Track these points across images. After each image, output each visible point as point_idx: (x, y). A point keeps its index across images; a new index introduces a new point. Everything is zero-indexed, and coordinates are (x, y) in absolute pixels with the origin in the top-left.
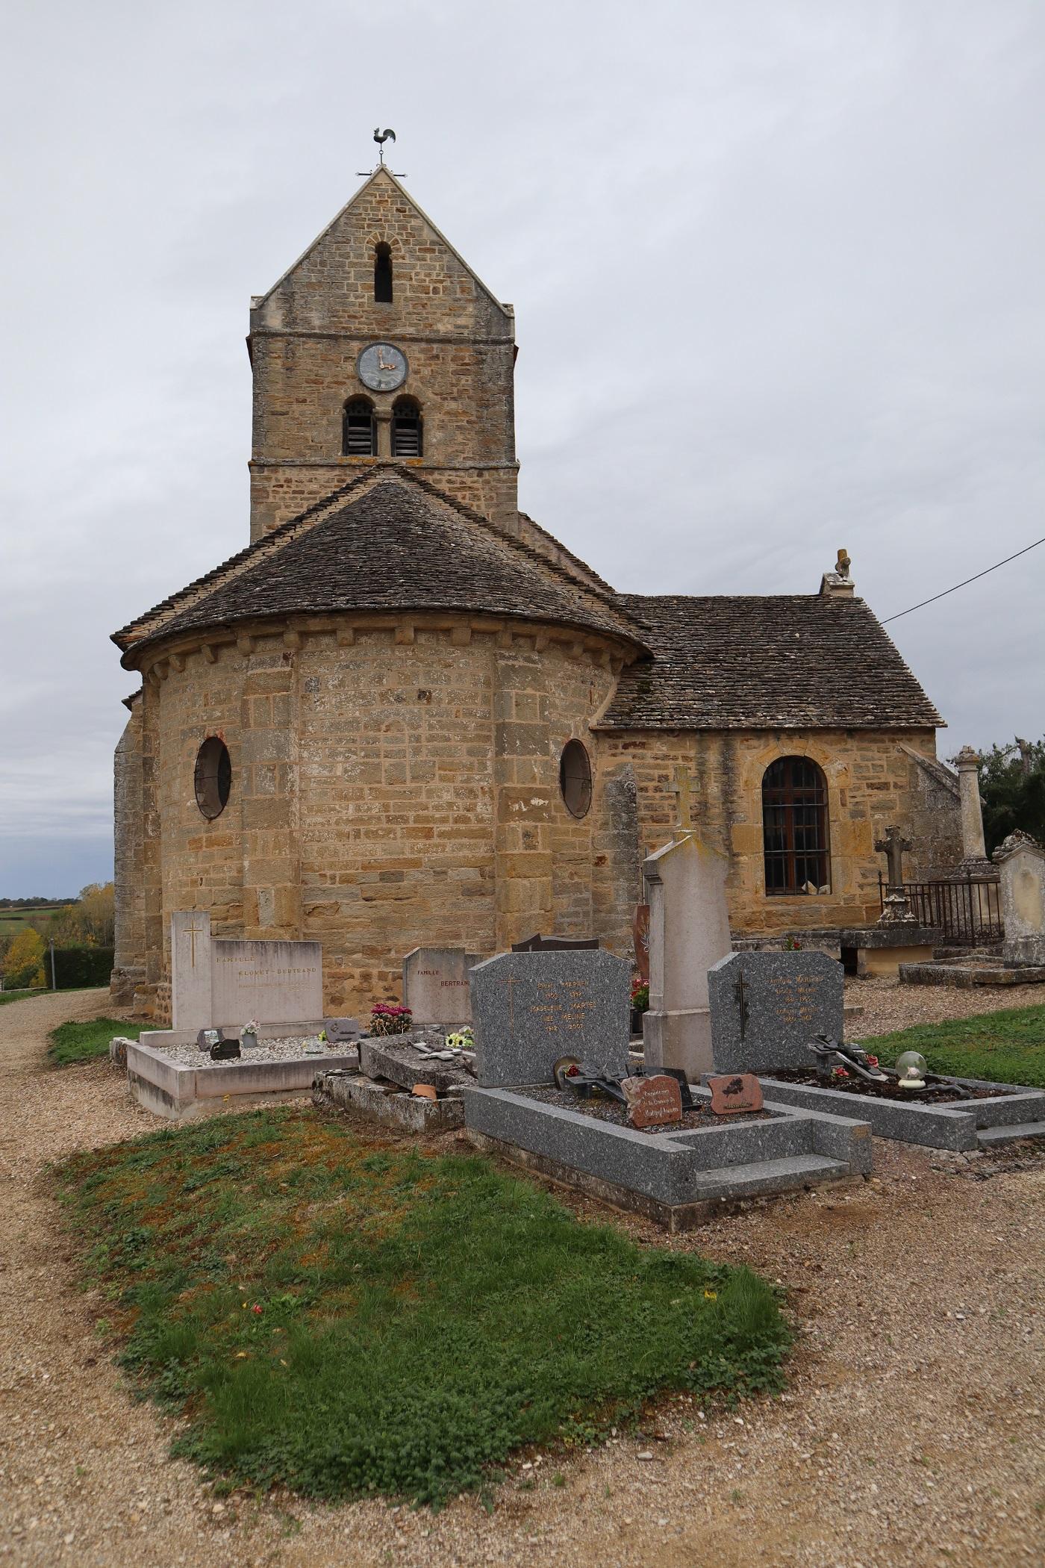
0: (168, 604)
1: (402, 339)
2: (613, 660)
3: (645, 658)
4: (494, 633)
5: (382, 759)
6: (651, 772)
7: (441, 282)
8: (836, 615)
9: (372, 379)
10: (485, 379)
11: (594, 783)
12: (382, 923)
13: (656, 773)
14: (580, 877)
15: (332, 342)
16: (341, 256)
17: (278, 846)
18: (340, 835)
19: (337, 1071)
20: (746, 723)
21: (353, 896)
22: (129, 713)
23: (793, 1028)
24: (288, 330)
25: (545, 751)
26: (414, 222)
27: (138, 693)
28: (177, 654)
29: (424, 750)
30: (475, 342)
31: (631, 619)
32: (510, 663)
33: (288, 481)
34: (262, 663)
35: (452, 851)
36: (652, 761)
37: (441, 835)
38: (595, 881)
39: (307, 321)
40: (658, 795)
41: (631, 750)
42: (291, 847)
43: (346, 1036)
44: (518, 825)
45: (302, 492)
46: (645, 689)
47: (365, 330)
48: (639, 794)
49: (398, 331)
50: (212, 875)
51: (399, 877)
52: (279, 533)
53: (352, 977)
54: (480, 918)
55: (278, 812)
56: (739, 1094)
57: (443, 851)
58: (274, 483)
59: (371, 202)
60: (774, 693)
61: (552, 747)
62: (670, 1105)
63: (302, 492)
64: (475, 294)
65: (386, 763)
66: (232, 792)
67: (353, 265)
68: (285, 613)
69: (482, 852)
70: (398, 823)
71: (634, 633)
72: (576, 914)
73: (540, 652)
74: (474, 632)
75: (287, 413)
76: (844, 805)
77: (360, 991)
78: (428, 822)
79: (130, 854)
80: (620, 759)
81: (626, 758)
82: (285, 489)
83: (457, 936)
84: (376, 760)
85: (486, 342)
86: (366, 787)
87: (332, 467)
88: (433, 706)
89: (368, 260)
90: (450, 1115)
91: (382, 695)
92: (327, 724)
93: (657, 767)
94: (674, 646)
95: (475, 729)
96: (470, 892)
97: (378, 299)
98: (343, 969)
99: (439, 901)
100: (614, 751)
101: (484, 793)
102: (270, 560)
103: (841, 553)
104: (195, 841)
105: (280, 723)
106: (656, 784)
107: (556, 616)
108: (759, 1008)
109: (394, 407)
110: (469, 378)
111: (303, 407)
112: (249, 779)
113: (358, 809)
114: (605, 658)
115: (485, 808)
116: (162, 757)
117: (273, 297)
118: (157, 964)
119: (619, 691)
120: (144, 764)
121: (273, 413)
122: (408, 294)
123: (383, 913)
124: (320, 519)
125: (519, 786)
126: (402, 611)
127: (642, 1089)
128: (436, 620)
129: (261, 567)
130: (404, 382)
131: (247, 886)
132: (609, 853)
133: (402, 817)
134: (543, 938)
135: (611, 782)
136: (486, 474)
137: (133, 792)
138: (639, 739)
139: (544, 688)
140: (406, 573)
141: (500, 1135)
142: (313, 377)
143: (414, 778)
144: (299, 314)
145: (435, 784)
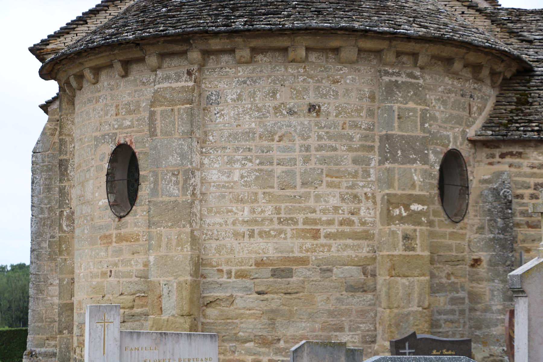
2: (493, 74)
3: (525, 71)
5: (275, 167)
6: (527, 180)
11: (471, 190)
12: (273, 315)
13: (532, 181)
14: (456, 277)
17: (180, 243)
18: (236, 235)
21: (247, 290)
22: (46, 117)
25: (425, 160)
27: (54, 99)
28: (90, 68)
29: (314, 160)
31: (512, 33)
32: (394, 79)
34: (168, 78)
35: (336, 249)
36: (528, 170)
37: (328, 236)
38: (472, 281)
41: (508, 160)
42: (192, 245)
44: (399, 229)
46: (523, 101)
48: (515, 201)
50: (121, 268)
51: (289, 273)
54: (362, 313)
55: (186, 212)
57: (329, 251)
61: (432, 157)
65: (278, 170)
66: (140, 193)
68: (189, 33)
69: (364, 252)
70: (288, 224)
71: (513, 47)
72: (452, 312)
73: (422, 68)
74: (360, 51)
78: (316, 224)
79: (45, 245)
80: (497, 168)
81: (503, 166)
83: (341, 329)
84: (269, 168)
86: (260, 192)
88: (322, 120)
91: (275, 108)
92: (226, 134)
93: (533, 175)
95: (360, 140)
96: (354, 289)
99: (325, 297)
100: (491, 160)
101: (367, 198)
104: (106, 237)
105: (183, 132)
107: (437, 34)
112: (156, 183)
113: (253, 211)
114: (485, 72)
115: (368, 212)
116: (76, 160)
118: (68, 348)
123: (273, 306)
125: (400, 192)
126: (295, 32)
131: (152, 279)
132: (484, 256)
133: (292, 219)
134: (419, 336)
135: (487, 189)
137: (48, 188)
138: (516, 149)
139: (425, 102)
143: (304, 184)
145: (322, 189)
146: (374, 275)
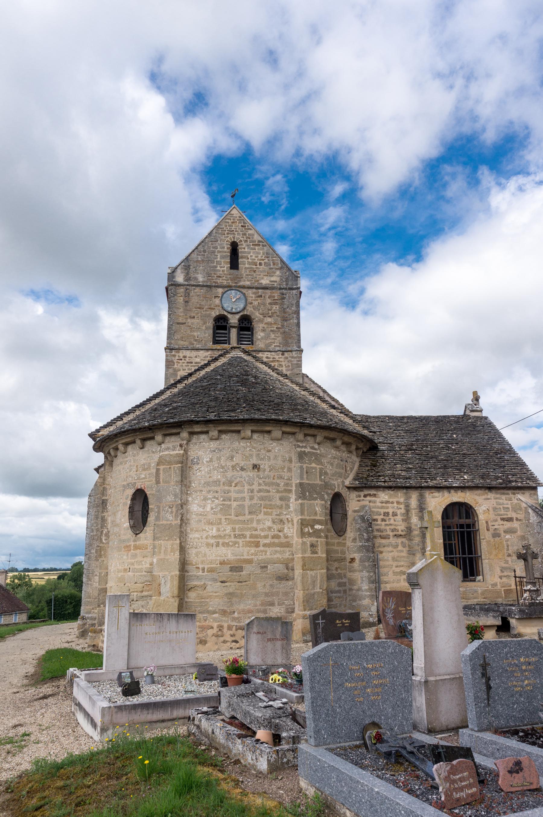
0: (120, 418)
1: (244, 287)
2: (357, 449)
4: (294, 434)
5: (232, 502)
6: (380, 510)
7: (263, 260)
8: (474, 425)
9: (228, 307)
10: (285, 306)
11: (348, 516)
13: (382, 511)
14: (341, 569)
15: (209, 289)
16: (213, 248)
18: (208, 545)
19: (205, 709)
20: (431, 484)
21: (215, 580)
23: (521, 695)
24: (186, 283)
26: (250, 232)
27: (103, 465)
28: (122, 444)
30: (280, 289)
32: (303, 449)
33: (185, 357)
34: (168, 449)
35: (269, 554)
36: (380, 505)
37: (265, 545)
39: (196, 279)
40: (383, 523)
41: (368, 498)
43: (210, 677)
45: (192, 363)
47: (225, 283)
49: (241, 283)
50: (136, 567)
51: (240, 569)
52: (179, 382)
53: (212, 628)
56: (521, 774)
58: (177, 358)
59: (229, 223)
60: (445, 467)
62: (470, 786)
63: (192, 363)
64: (280, 265)
65: (234, 504)
66: (149, 519)
67: (219, 252)
68: (181, 422)
70: (240, 538)
71: (365, 432)
72: (339, 591)
73: (319, 444)
74: (283, 433)
75: (185, 323)
76: (488, 530)
77: (217, 636)
78: (257, 538)
79: (93, 551)
81: (366, 502)
82: (183, 361)
83: (272, 604)
84: (229, 503)
85: (286, 289)
87: (208, 350)
88: (261, 474)
89: (227, 249)
90: (285, 760)
92: (203, 482)
93: (382, 507)
94: (389, 442)
95: (284, 486)
97: (231, 268)
98: (207, 623)
100: (359, 499)
101: (288, 521)
102: (175, 395)
103: (475, 393)
104: (127, 546)
106: (382, 517)
107: (327, 424)
108: (497, 681)
109: (239, 321)
110: (277, 306)
111: (193, 320)
112: (159, 512)
113: (218, 530)
116: (112, 499)
117: (180, 267)
119: (360, 466)
120: (103, 503)
121: (178, 324)
122: (247, 266)
123: (231, 590)
124: (201, 375)
125: (308, 518)
127: (449, 773)
128: (262, 425)
129: (169, 398)
130: (244, 308)
132: (357, 556)
133: (242, 535)
136: (286, 354)
137: (97, 517)
138: (372, 492)
139: (322, 464)
140: (246, 401)
141: (327, 791)
142: (198, 306)
143: (250, 513)
144: (192, 275)
146: (293, 570)
